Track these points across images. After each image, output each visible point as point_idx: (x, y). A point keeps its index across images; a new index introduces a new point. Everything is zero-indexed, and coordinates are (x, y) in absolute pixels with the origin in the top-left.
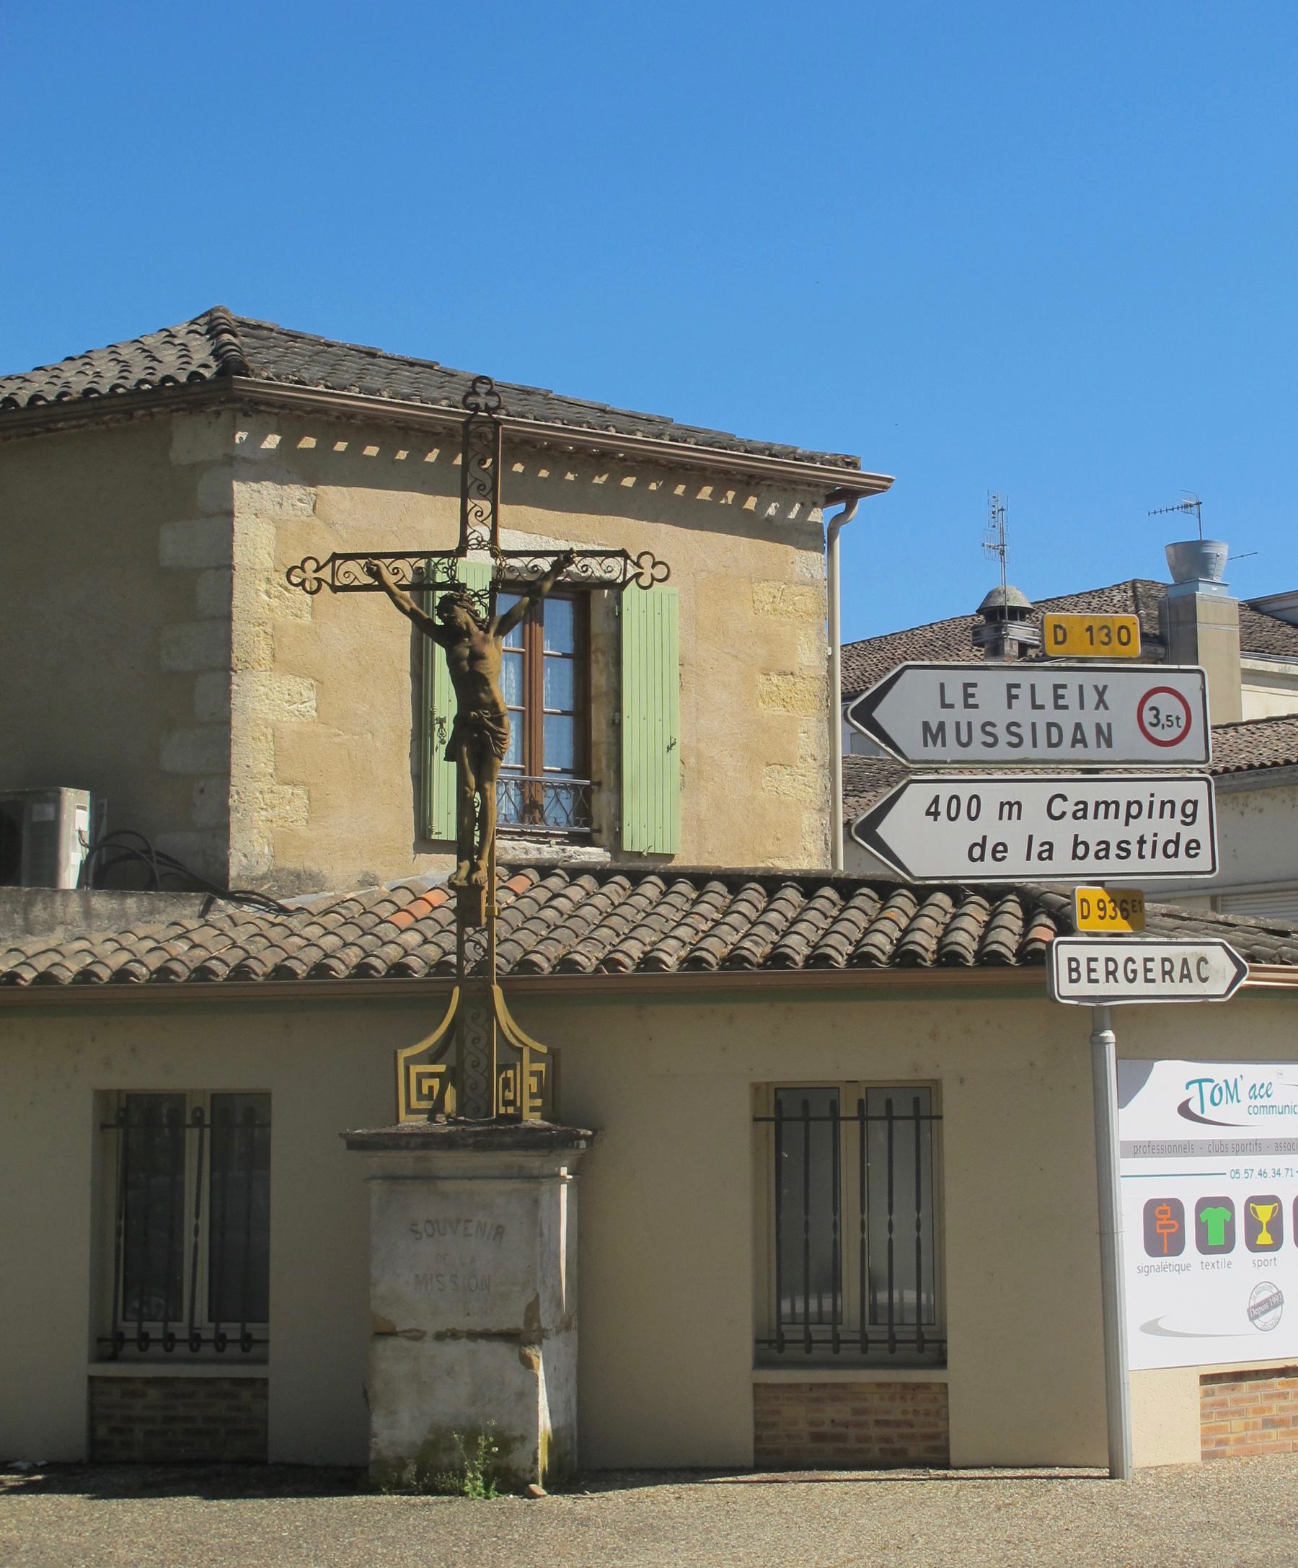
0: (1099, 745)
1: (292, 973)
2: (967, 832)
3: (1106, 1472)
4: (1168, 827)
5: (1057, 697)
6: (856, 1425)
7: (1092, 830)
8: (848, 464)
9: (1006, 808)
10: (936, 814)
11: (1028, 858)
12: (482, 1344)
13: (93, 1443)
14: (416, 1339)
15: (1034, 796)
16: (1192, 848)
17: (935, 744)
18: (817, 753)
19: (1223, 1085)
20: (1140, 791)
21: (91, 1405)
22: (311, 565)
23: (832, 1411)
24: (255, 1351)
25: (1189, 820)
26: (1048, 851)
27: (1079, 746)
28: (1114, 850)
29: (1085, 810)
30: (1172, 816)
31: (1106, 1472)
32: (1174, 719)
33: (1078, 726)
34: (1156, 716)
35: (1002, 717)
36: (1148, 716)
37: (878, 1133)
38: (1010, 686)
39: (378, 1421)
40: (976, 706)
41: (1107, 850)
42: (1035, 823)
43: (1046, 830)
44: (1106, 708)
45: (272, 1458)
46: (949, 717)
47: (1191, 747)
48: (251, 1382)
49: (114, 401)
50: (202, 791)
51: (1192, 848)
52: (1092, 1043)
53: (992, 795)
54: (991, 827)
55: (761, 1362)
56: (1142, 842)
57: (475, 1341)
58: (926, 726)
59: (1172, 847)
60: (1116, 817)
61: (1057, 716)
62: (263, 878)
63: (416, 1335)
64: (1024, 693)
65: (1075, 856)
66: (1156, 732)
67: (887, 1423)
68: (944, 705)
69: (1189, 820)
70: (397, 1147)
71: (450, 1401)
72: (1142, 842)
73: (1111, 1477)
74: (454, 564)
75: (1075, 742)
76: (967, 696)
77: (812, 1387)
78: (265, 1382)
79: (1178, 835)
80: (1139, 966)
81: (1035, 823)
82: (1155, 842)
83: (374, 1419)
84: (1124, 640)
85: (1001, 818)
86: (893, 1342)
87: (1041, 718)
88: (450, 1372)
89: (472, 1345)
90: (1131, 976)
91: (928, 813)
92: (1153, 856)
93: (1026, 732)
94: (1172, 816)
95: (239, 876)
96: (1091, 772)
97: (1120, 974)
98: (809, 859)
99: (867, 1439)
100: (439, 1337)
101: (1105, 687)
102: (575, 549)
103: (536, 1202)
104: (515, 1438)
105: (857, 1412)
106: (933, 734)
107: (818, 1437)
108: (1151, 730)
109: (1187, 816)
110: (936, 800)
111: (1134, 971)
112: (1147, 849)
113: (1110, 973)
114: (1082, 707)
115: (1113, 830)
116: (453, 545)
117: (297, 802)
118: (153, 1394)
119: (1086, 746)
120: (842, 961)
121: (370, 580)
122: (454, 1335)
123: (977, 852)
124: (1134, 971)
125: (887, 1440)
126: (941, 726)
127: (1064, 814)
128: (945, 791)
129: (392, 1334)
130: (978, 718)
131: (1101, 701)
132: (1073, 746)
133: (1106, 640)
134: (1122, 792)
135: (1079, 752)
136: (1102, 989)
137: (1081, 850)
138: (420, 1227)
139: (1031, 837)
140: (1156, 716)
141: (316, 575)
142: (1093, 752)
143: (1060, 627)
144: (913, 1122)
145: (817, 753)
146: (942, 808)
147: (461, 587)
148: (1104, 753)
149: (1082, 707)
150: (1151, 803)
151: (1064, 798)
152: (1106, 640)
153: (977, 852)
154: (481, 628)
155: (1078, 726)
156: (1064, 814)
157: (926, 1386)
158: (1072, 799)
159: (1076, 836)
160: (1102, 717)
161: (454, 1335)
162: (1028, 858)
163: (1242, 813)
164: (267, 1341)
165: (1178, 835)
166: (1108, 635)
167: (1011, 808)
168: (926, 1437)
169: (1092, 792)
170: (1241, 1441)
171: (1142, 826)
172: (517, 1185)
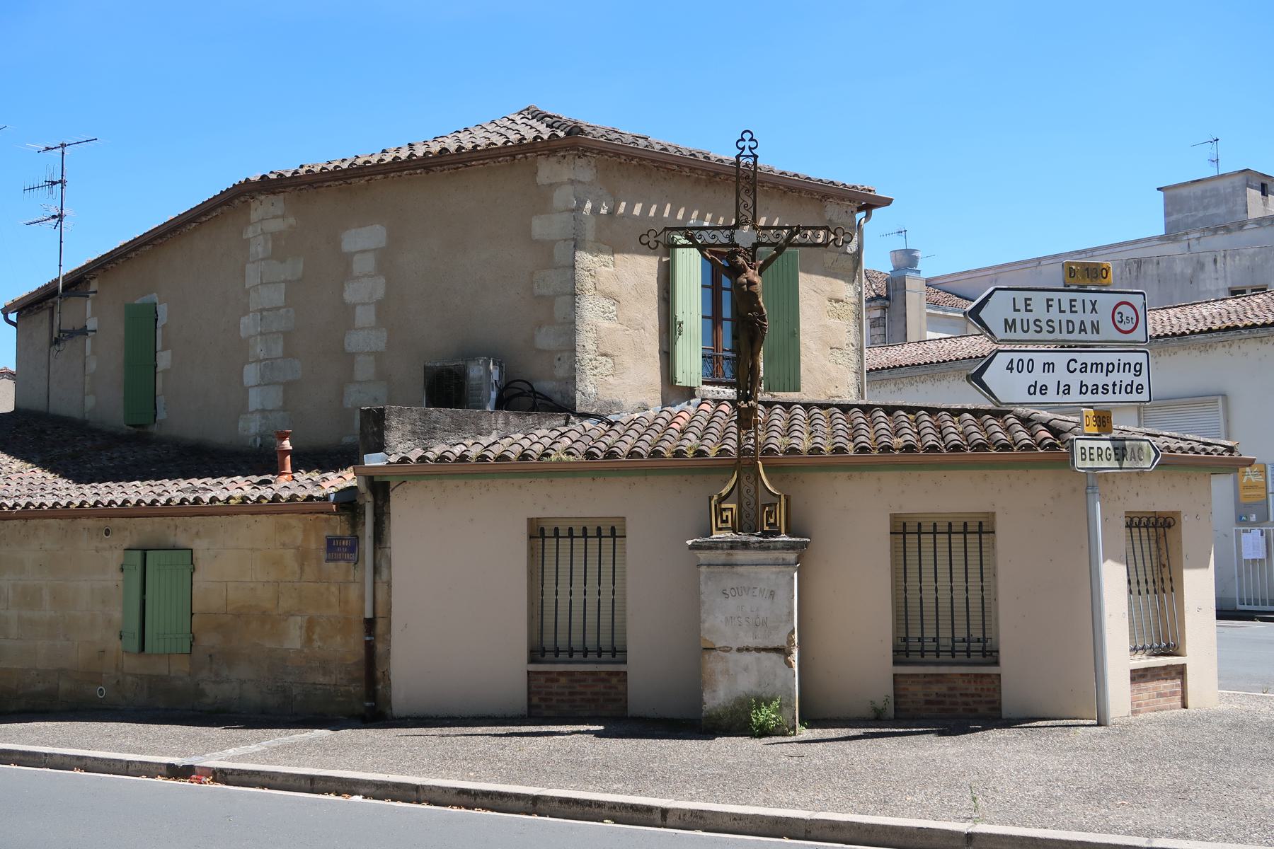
1: (507, 458)
2: (1026, 379)
3: (1095, 722)
4: (1127, 377)
5: (1072, 306)
6: (950, 696)
7: (1091, 378)
10: (1012, 369)
12: (763, 653)
13: (530, 706)
15: (1061, 359)
16: (1140, 388)
18: (853, 341)
20: (1113, 358)
21: (529, 688)
22: (652, 234)
23: (936, 689)
24: (618, 657)
28: (1100, 389)
31: (1095, 722)
33: (1082, 322)
35: (1044, 317)
36: (1117, 317)
37: (592, 543)
38: (1048, 300)
39: (707, 696)
42: (1061, 374)
43: (1067, 378)
46: (1017, 316)
47: (1138, 335)
48: (617, 673)
49: (475, 155)
51: (1140, 388)
53: (1040, 359)
54: (1039, 376)
55: (896, 663)
56: (1114, 385)
58: (1006, 321)
59: (1129, 389)
63: (727, 649)
64: (1055, 304)
66: (1121, 326)
67: (966, 695)
68: (1015, 310)
70: (717, 548)
71: (746, 684)
72: (1114, 385)
73: (1099, 725)
75: (1081, 331)
76: (1027, 305)
77: (925, 675)
81: (1061, 374)
86: (968, 652)
87: (1064, 317)
88: (746, 669)
93: (1056, 325)
96: (1086, 347)
98: (850, 397)
99: (956, 703)
100: (739, 650)
105: (951, 689)
106: (1009, 325)
107: (928, 702)
113: (1100, 456)
115: (1099, 378)
117: (609, 366)
118: (563, 680)
120: (601, 455)
122: (748, 649)
123: (1032, 390)
125: (967, 704)
126: (1014, 321)
128: (1016, 356)
130: (1032, 317)
131: (1094, 309)
134: (1105, 358)
135: (1083, 336)
136: (1096, 464)
137: (1084, 389)
142: (1090, 336)
144: (977, 536)
145: (853, 341)
146: (1015, 365)
147: (737, 246)
148: (1095, 337)
153: (1032, 390)
155: (1082, 322)
157: (989, 675)
160: (1094, 317)
161: (748, 649)
167: (1049, 366)
168: (987, 702)
169: (1089, 358)
170: (1147, 704)
171: (1115, 377)
172: (783, 569)
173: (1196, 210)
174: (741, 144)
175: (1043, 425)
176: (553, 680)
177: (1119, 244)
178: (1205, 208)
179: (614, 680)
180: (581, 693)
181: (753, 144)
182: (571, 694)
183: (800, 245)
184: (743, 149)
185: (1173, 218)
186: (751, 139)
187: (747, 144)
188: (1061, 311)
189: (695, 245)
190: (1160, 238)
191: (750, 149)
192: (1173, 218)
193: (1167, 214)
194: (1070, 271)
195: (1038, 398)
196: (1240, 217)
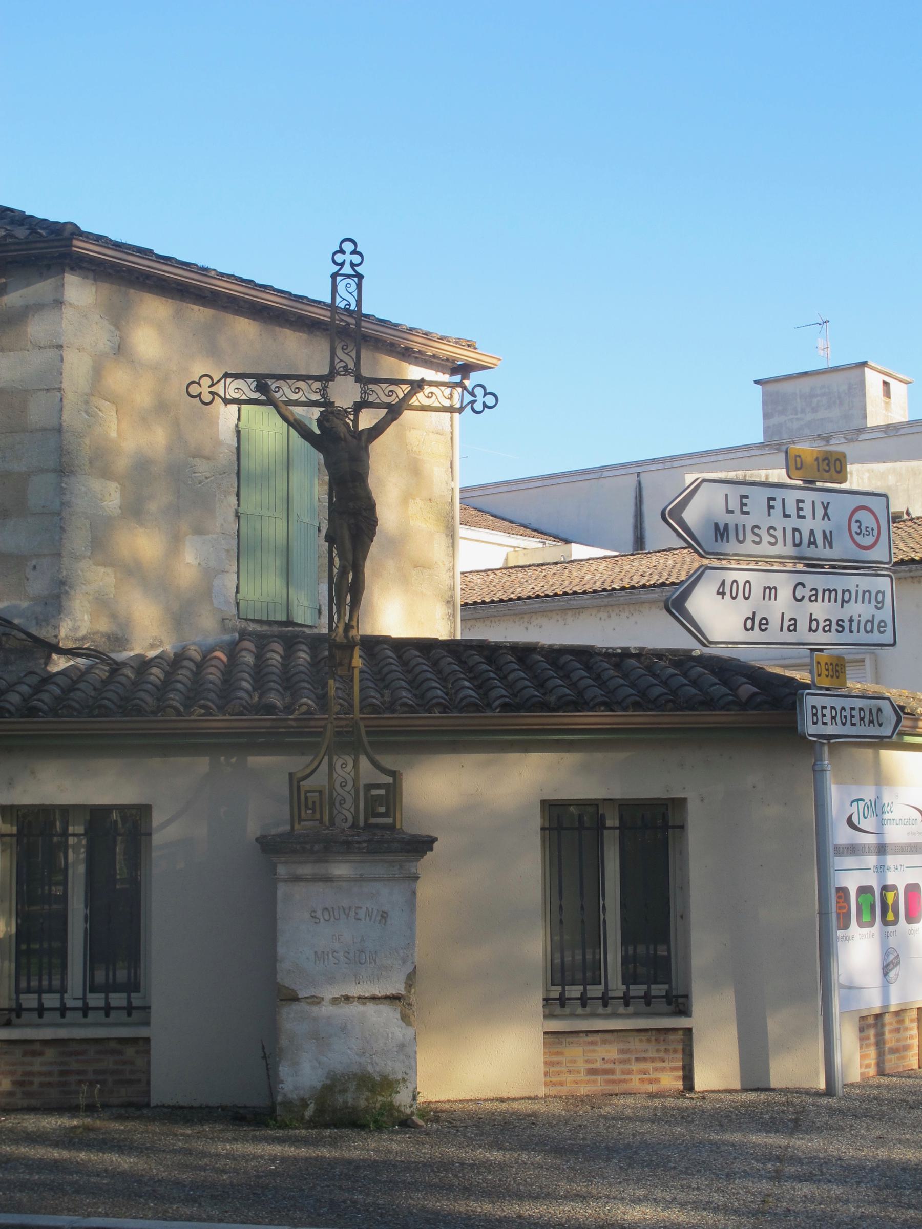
0: (825, 547)
5: (799, 509)
8: (469, 346)
9: (768, 591)
11: (781, 630)
14: (313, 1003)
17: (722, 540)
19: (869, 803)
25: (879, 605)
26: (793, 626)
27: (812, 546)
28: (834, 627)
29: (816, 595)
30: (870, 602)
32: (869, 529)
34: (859, 527)
36: (855, 527)
38: (770, 499)
39: (284, 1070)
40: (747, 513)
41: (830, 625)
44: (829, 519)
45: (153, 1103)
46: (730, 520)
48: (134, 1041)
50: (35, 567)
52: (814, 771)
56: (851, 620)
57: (365, 1004)
60: (836, 601)
61: (798, 523)
62: (84, 638)
64: (777, 504)
65: (810, 630)
69: (879, 605)
72: (851, 620)
74: (325, 388)
76: (743, 505)
78: (147, 1040)
79: (873, 616)
80: (847, 713)
82: (859, 621)
83: (281, 1068)
84: (838, 469)
85: (764, 598)
89: (361, 1008)
90: (844, 720)
91: (718, 593)
92: (858, 632)
94: (870, 602)
95: (67, 637)
97: (838, 719)
101: (828, 503)
102: (427, 379)
103: (414, 893)
104: (398, 1082)
108: (855, 536)
109: (878, 602)
110: (723, 583)
111: (845, 717)
112: (855, 625)
114: (814, 518)
116: (325, 371)
118: (50, 1053)
119: (817, 547)
121: (256, 396)
124: (845, 717)
126: (726, 526)
127: (803, 597)
129: (295, 999)
131: (826, 514)
132: (809, 547)
133: (827, 468)
137: (814, 626)
138: (319, 914)
139: (783, 614)
140: (859, 527)
141: (210, 389)
143: (799, 456)
146: (727, 590)
148: (827, 553)
149: (814, 518)
150: (857, 591)
151: (804, 586)
152: (827, 468)
154: (353, 437)
156: (803, 597)
158: (809, 586)
159: (811, 615)
162: (781, 630)
163: (527, 629)
164: (149, 1008)
165: (873, 616)
166: (828, 465)
173: (803, 411)
174: (339, 258)
175: (744, 676)
176: (34, 1054)
177: (707, 453)
178: (815, 410)
179: (130, 1051)
180: (79, 1073)
181: (356, 259)
182: (63, 1073)
183: (423, 408)
184: (342, 265)
185: (777, 420)
186: (354, 252)
187: (348, 257)
188: (786, 516)
189: (270, 402)
190: (761, 446)
191: (353, 265)
192: (777, 420)
193: (766, 416)
194: (63, 583)
195: (756, 635)
196: (856, 424)
